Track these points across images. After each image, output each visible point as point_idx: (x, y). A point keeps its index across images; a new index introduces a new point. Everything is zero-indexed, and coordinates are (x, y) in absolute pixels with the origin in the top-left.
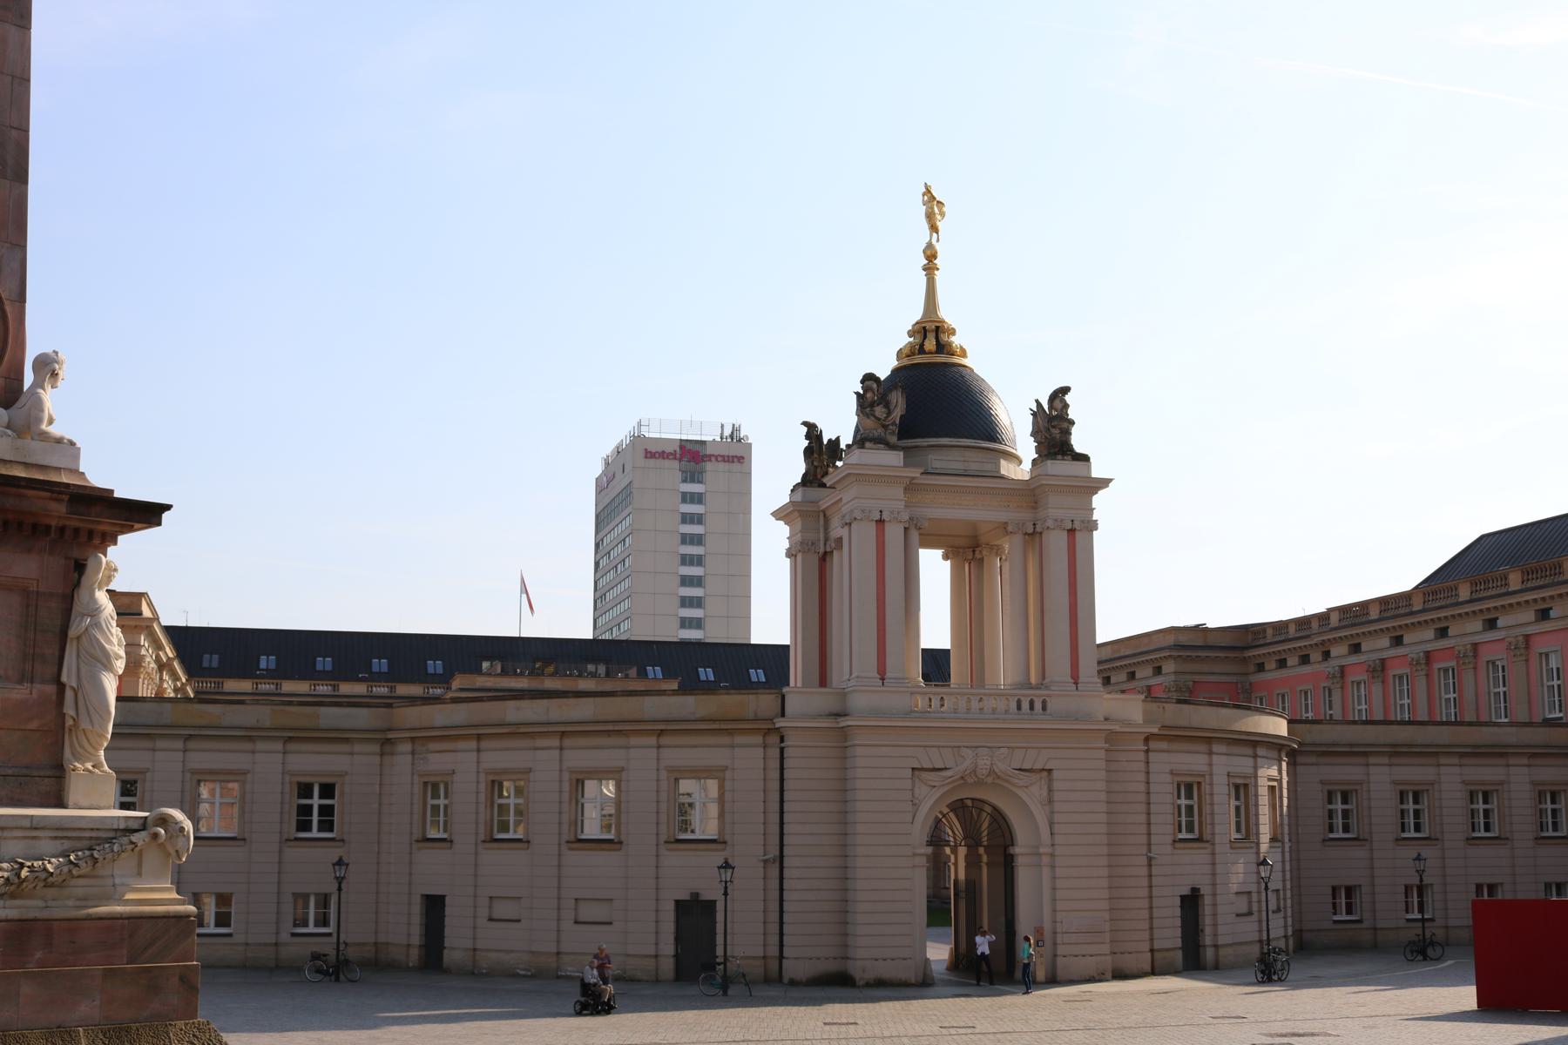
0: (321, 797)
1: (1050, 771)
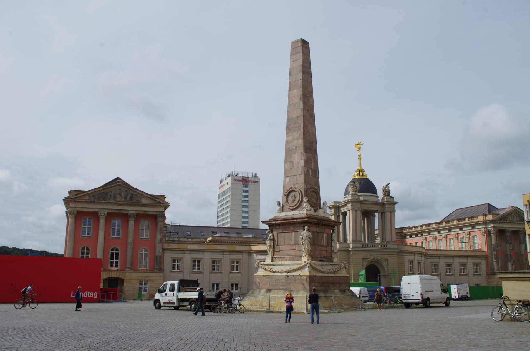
0: (115, 260)
1: (387, 259)
